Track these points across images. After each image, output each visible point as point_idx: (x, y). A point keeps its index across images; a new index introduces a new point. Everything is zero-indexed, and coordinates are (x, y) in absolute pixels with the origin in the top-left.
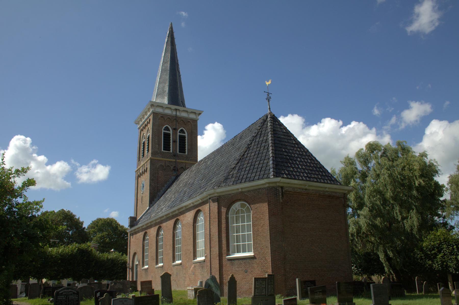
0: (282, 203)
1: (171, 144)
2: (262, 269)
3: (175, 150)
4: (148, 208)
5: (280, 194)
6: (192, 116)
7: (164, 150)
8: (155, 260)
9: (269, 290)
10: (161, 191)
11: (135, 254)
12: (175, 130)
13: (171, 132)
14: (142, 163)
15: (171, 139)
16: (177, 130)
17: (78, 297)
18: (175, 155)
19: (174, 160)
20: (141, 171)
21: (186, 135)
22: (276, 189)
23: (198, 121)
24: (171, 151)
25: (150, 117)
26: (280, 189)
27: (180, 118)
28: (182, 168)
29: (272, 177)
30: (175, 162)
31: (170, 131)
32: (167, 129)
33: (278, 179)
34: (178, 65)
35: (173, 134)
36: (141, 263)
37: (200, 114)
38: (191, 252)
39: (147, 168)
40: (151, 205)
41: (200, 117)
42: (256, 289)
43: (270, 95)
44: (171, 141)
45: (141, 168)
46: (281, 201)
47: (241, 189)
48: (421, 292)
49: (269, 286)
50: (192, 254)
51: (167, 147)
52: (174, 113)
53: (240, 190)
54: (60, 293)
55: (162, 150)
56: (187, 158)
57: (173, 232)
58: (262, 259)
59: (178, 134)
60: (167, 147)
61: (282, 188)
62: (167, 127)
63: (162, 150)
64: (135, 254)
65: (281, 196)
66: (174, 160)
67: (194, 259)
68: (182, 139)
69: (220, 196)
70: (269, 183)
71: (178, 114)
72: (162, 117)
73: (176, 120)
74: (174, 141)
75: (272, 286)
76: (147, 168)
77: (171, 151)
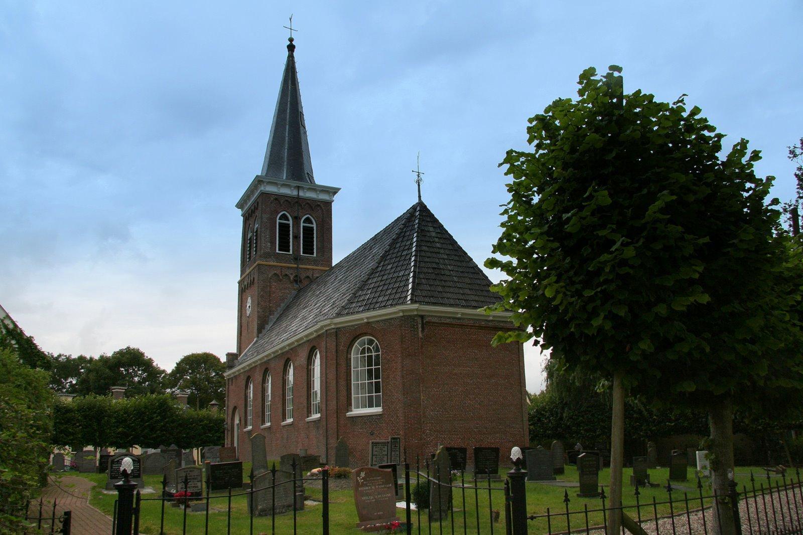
0: (421, 339)
1: (291, 240)
2: (392, 430)
3: (296, 250)
4: (255, 339)
5: (420, 326)
6: (324, 197)
7: (279, 250)
8: (261, 418)
9: (393, 459)
10: (276, 313)
11: (235, 408)
12: (296, 219)
13: (291, 222)
14: (248, 271)
15: (291, 233)
16: (300, 219)
17: (140, 465)
18: (296, 258)
19: (296, 266)
20: (246, 283)
21: (314, 226)
22: (414, 320)
23: (333, 204)
24: (291, 252)
25: (258, 200)
26: (419, 321)
27: (304, 199)
28: (308, 277)
29: (409, 302)
30: (297, 268)
31: (289, 221)
32: (284, 217)
33: (416, 306)
34: (301, 114)
35: (293, 224)
36: (243, 422)
37: (335, 193)
38: (304, 406)
39: (254, 278)
40: (260, 335)
41: (336, 197)
42: (374, 457)
43: (421, 175)
44: (291, 236)
45: (247, 278)
46: (420, 335)
47: (367, 318)
48: (59, 454)
49: (393, 453)
50: (305, 410)
51: (284, 246)
52: (295, 193)
53: (365, 320)
54: (115, 460)
55: (277, 251)
56: (315, 262)
57: (283, 378)
58: (392, 417)
59: (302, 224)
60: (284, 246)
61: (422, 317)
62: (284, 214)
63: (277, 251)
64: (235, 408)
65: (420, 329)
66: (296, 266)
67: (308, 417)
68: (308, 232)
69: (339, 328)
70: (403, 311)
71: (301, 194)
72: (276, 199)
73: (296, 204)
74: (296, 237)
75: (398, 453)
76: (254, 278)
77: (291, 252)
